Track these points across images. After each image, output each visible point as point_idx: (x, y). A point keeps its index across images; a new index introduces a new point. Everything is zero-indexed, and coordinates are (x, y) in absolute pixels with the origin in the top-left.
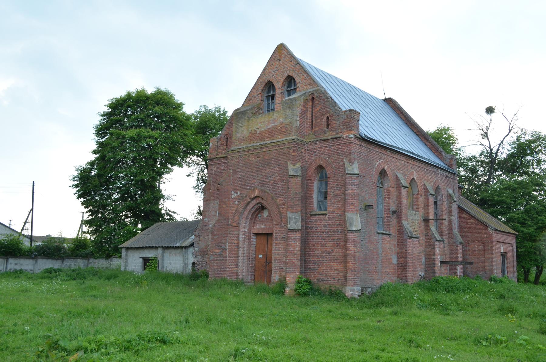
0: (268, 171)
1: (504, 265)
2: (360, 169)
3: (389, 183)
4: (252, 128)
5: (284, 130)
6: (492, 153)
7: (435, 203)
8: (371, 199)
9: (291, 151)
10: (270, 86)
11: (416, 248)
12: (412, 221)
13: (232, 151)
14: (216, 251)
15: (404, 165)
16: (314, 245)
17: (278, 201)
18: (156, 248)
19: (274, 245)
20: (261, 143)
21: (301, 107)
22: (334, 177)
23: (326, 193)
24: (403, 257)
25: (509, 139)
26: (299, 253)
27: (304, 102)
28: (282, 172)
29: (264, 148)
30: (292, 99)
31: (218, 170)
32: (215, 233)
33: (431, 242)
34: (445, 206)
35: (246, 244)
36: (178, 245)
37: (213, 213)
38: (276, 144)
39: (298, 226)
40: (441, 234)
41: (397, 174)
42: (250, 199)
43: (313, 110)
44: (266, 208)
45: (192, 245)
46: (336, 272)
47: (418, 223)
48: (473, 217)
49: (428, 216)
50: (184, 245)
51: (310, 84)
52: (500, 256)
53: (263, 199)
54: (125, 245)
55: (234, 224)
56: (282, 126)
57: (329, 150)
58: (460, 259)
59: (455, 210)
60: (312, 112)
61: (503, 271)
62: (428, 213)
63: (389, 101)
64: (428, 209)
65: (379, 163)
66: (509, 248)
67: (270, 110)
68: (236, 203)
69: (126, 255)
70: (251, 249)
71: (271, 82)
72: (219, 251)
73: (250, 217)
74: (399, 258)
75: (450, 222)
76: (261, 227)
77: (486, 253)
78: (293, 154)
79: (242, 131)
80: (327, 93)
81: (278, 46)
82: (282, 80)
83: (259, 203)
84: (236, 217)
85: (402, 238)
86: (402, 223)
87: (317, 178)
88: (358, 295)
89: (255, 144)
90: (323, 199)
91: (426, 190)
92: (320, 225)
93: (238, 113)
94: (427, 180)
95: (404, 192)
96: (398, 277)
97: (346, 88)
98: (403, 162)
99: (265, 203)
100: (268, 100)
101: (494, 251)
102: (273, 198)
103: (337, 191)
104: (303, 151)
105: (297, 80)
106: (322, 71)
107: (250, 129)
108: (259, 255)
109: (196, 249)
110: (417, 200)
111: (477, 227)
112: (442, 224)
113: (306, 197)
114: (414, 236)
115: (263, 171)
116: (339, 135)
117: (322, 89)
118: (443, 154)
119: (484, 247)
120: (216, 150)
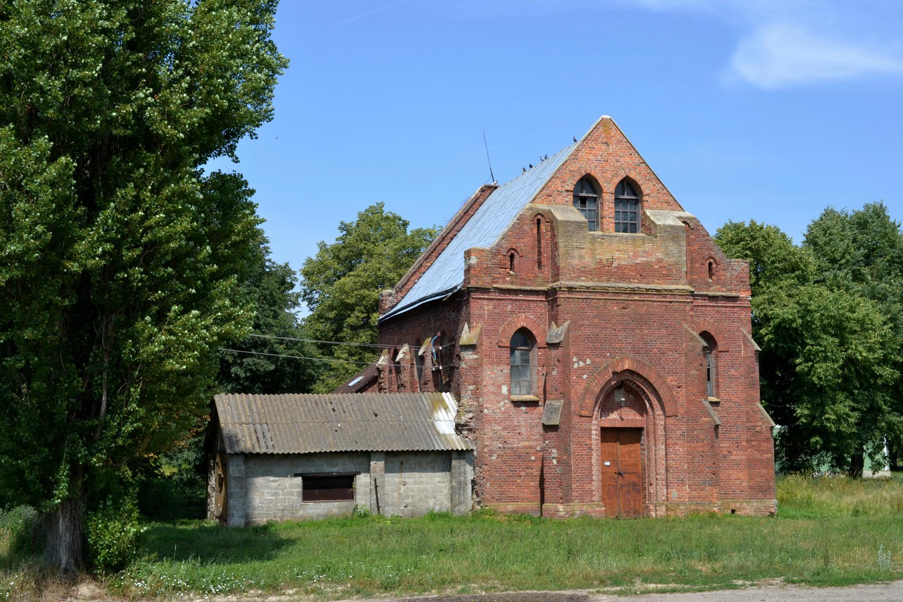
17: (668, 381)
31: (497, 311)
37: (491, 388)
46: (737, 482)
56: (661, 265)
57: (717, 312)
68: (585, 377)
78: (691, 313)
84: (587, 401)
107: (598, 257)
116: (734, 294)
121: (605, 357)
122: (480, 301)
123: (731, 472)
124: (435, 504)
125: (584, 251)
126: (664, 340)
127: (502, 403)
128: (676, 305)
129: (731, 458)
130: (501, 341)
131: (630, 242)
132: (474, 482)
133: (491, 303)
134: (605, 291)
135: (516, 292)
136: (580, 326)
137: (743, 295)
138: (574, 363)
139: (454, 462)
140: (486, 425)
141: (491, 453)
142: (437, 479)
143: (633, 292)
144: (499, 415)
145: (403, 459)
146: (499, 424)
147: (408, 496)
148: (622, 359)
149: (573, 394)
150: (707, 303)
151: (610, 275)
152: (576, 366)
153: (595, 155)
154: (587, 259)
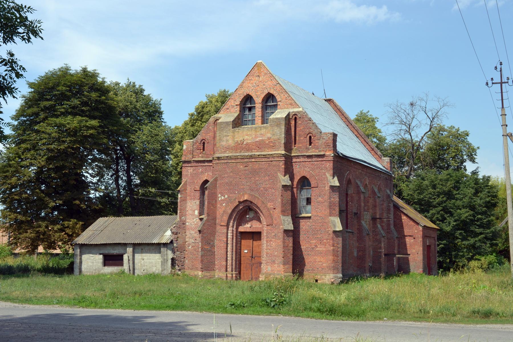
14: (206, 247)
17: (268, 205)
18: (125, 245)
28: (272, 181)
31: (194, 172)
33: (378, 237)
36: (155, 241)
37: (190, 212)
41: (357, 181)
46: (320, 263)
51: (291, 104)
57: (312, 164)
62: (375, 213)
68: (224, 205)
74: (358, 252)
84: (224, 217)
102: (263, 203)
103: (320, 199)
105: (278, 98)
107: (236, 140)
110: (368, 202)
116: (322, 153)
120: (192, 152)
121: (235, 194)
122: (187, 168)
124: (156, 270)
125: (229, 137)
126: (267, 183)
127: (195, 220)
128: (274, 163)
129: (317, 249)
130: (195, 188)
131: (253, 129)
132: (173, 259)
133: (192, 168)
134: (236, 158)
135: (204, 162)
136: (223, 178)
137: (327, 153)
138: (219, 197)
139: (162, 249)
140: (187, 231)
141: (189, 245)
142: (157, 258)
143: (251, 157)
144: (193, 226)
145: (142, 247)
146: (193, 230)
147: (144, 265)
148: (243, 195)
149: (218, 214)
150: (306, 160)
151: (242, 149)
152: (220, 199)
154: (231, 142)
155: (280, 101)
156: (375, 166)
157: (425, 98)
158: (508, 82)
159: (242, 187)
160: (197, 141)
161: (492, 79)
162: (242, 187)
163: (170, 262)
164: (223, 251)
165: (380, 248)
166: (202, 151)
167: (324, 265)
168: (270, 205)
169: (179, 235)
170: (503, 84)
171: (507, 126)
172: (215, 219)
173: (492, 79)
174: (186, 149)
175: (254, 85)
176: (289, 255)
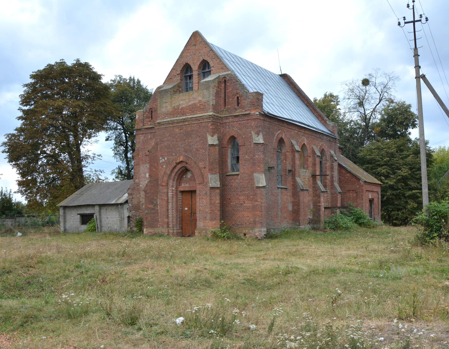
0: (190, 140)
1: (371, 208)
2: (264, 139)
3: (286, 149)
4: (175, 104)
5: (202, 107)
6: (366, 118)
7: (321, 162)
8: (272, 162)
9: (210, 124)
10: (187, 68)
11: (306, 199)
12: (303, 178)
13: (158, 123)
14: (149, 206)
15: (298, 134)
16: (230, 199)
17: (200, 165)
18: (93, 206)
19: (198, 200)
20: (184, 117)
21: (216, 88)
22: (244, 145)
23: (238, 158)
24: (296, 204)
25: (381, 107)
26: (219, 205)
27: (219, 84)
28: (202, 141)
29: (186, 121)
30: (208, 81)
31: (145, 139)
32: (148, 191)
34: (328, 164)
35: (175, 199)
36: (113, 202)
37: (143, 175)
38: (196, 119)
39: (218, 184)
40: (325, 186)
41: (292, 141)
42: (176, 163)
43: (225, 91)
44: (189, 171)
45: (126, 202)
46: (248, 218)
47: (308, 178)
48: (349, 172)
49: (315, 173)
50: (120, 201)
52: (368, 202)
53: (187, 163)
54: (63, 203)
55: (164, 184)
56: (201, 103)
57: (240, 124)
58: (339, 205)
59: (336, 167)
60: (225, 92)
61: (371, 213)
62: (315, 171)
63: (285, 77)
64: (315, 168)
65: (278, 134)
66: (375, 195)
67: (188, 89)
68: (164, 166)
69: (64, 213)
70: (179, 203)
71: (189, 64)
72: (152, 206)
73: (176, 178)
74: (293, 206)
75: (332, 177)
76: (185, 186)
77: (358, 200)
79: (165, 107)
80: (237, 77)
81: (193, 33)
82: (199, 63)
83: (183, 167)
84: (165, 178)
85: (296, 191)
86: (296, 179)
87: (230, 146)
88: (265, 235)
89: (178, 118)
90: (235, 162)
91: (314, 152)
92: (235, 183)
93: (159, 90)
94: (315, 145)
95: (297, 155)
96: (293, 220)
97: (250, 68)
98: (297, 132)
99: (189, 167)
100: (186, 79)
101: (364, 197)
102: (195, 163)
103: (247, 157)
104: (219, 124)
105: (211, 64)
106: (230, 53)
107: (173, 105)
108: (185, 207)
109: (130, 205)
110: (307, 161)
111: (352, 180)
112: (326, 179)
113: (222, 161)
114: (305, 189)
115: (186, 141)
116: (248, 112)
117: (233, 74)
118: (328, 122)
119: (357, 195)
120: (143, 121)
121: (173, 156)
123: (244, 213)
128: (204, 124)
129: (245, 205)
132: (129, 217)
138: (160, 160)
152: (161, 161)
153: (190, 53)
155: (213, 66)
156: (320, 130)
157: (374, 75)
158: (420, 21)
159: (178, 149)
160: (146, 111)
161: (404, 18)
162: (178, 149)
163: (126, 221)
164: (164, 209)
165: (320, 202)
166: (150, 119)
167: (251, 220)
168: (201, 165)
169: (134, 196)
170: (413, 20)
171: (420, 67)
172: (157, 180)
173: (404, 18)
174: (139, 118)
175: (192, 53)
176: (216, 211)
